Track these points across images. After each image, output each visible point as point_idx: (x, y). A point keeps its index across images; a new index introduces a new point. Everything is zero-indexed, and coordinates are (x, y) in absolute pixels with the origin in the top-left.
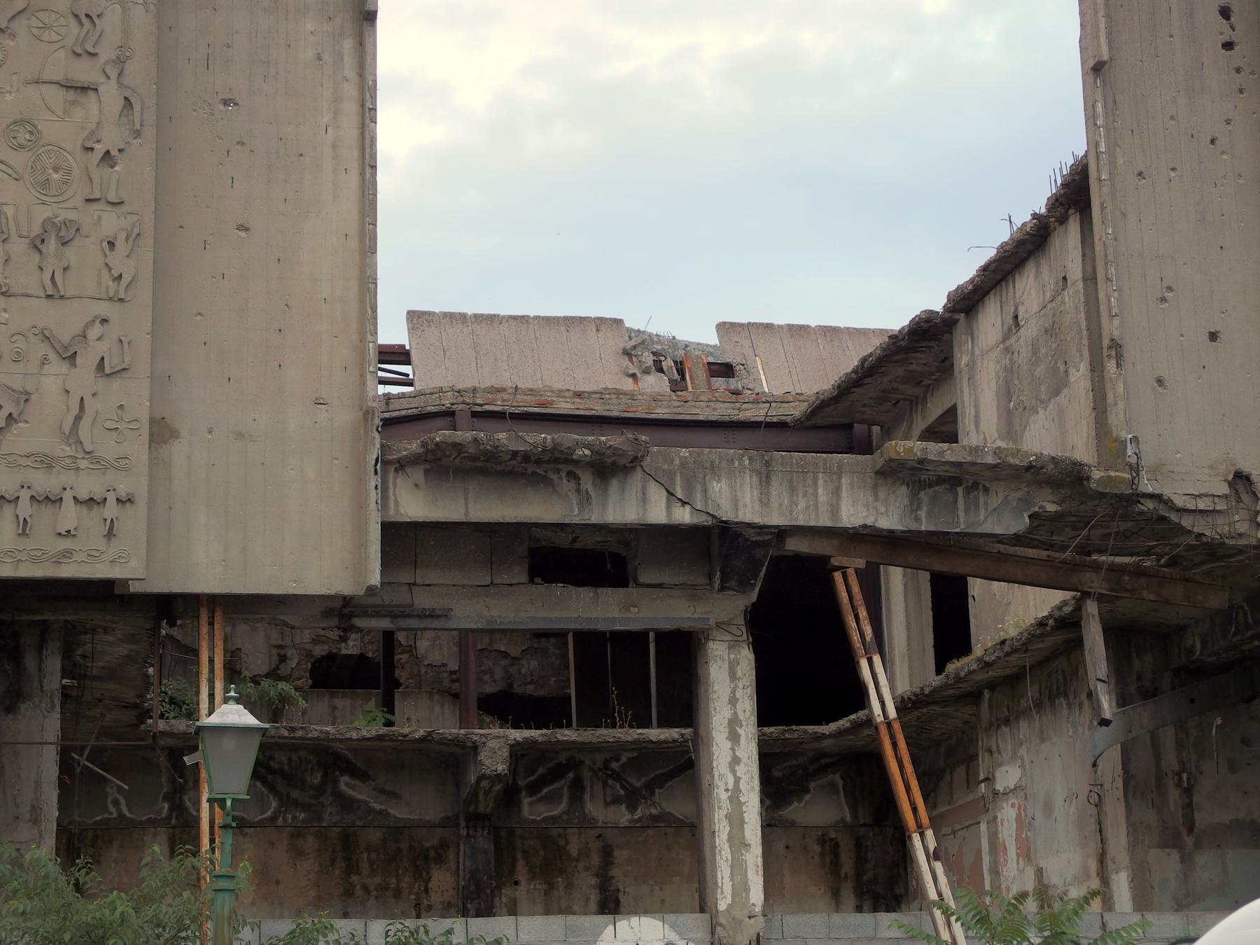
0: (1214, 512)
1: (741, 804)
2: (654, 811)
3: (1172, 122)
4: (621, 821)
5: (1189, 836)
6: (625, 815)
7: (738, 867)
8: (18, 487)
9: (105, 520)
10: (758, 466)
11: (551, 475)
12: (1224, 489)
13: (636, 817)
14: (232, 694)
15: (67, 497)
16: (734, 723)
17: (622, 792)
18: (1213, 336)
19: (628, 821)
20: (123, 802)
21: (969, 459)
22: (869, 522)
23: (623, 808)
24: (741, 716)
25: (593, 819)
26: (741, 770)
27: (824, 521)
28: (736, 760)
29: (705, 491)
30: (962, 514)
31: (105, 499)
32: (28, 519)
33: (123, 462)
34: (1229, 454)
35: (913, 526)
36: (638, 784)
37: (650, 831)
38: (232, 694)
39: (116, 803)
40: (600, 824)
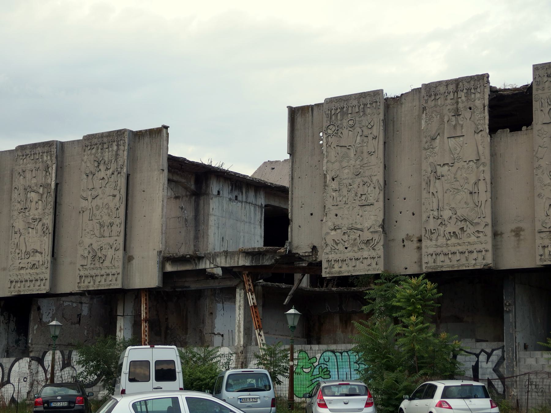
1: (240, 323)
7: (239, 337)
10: (225, 254)
11: (191, 260)
16: (240, 306)
18: (312, 214)
20: (329, 308)
21: (253, 251)
22: (244, 264)
24: (241, 305)
26: (240, 316)
27: (236, 265)
28: (240, 314)
29: (216, 261)
30: (261, 261)
35: (252, 264)
39: (328, 308)
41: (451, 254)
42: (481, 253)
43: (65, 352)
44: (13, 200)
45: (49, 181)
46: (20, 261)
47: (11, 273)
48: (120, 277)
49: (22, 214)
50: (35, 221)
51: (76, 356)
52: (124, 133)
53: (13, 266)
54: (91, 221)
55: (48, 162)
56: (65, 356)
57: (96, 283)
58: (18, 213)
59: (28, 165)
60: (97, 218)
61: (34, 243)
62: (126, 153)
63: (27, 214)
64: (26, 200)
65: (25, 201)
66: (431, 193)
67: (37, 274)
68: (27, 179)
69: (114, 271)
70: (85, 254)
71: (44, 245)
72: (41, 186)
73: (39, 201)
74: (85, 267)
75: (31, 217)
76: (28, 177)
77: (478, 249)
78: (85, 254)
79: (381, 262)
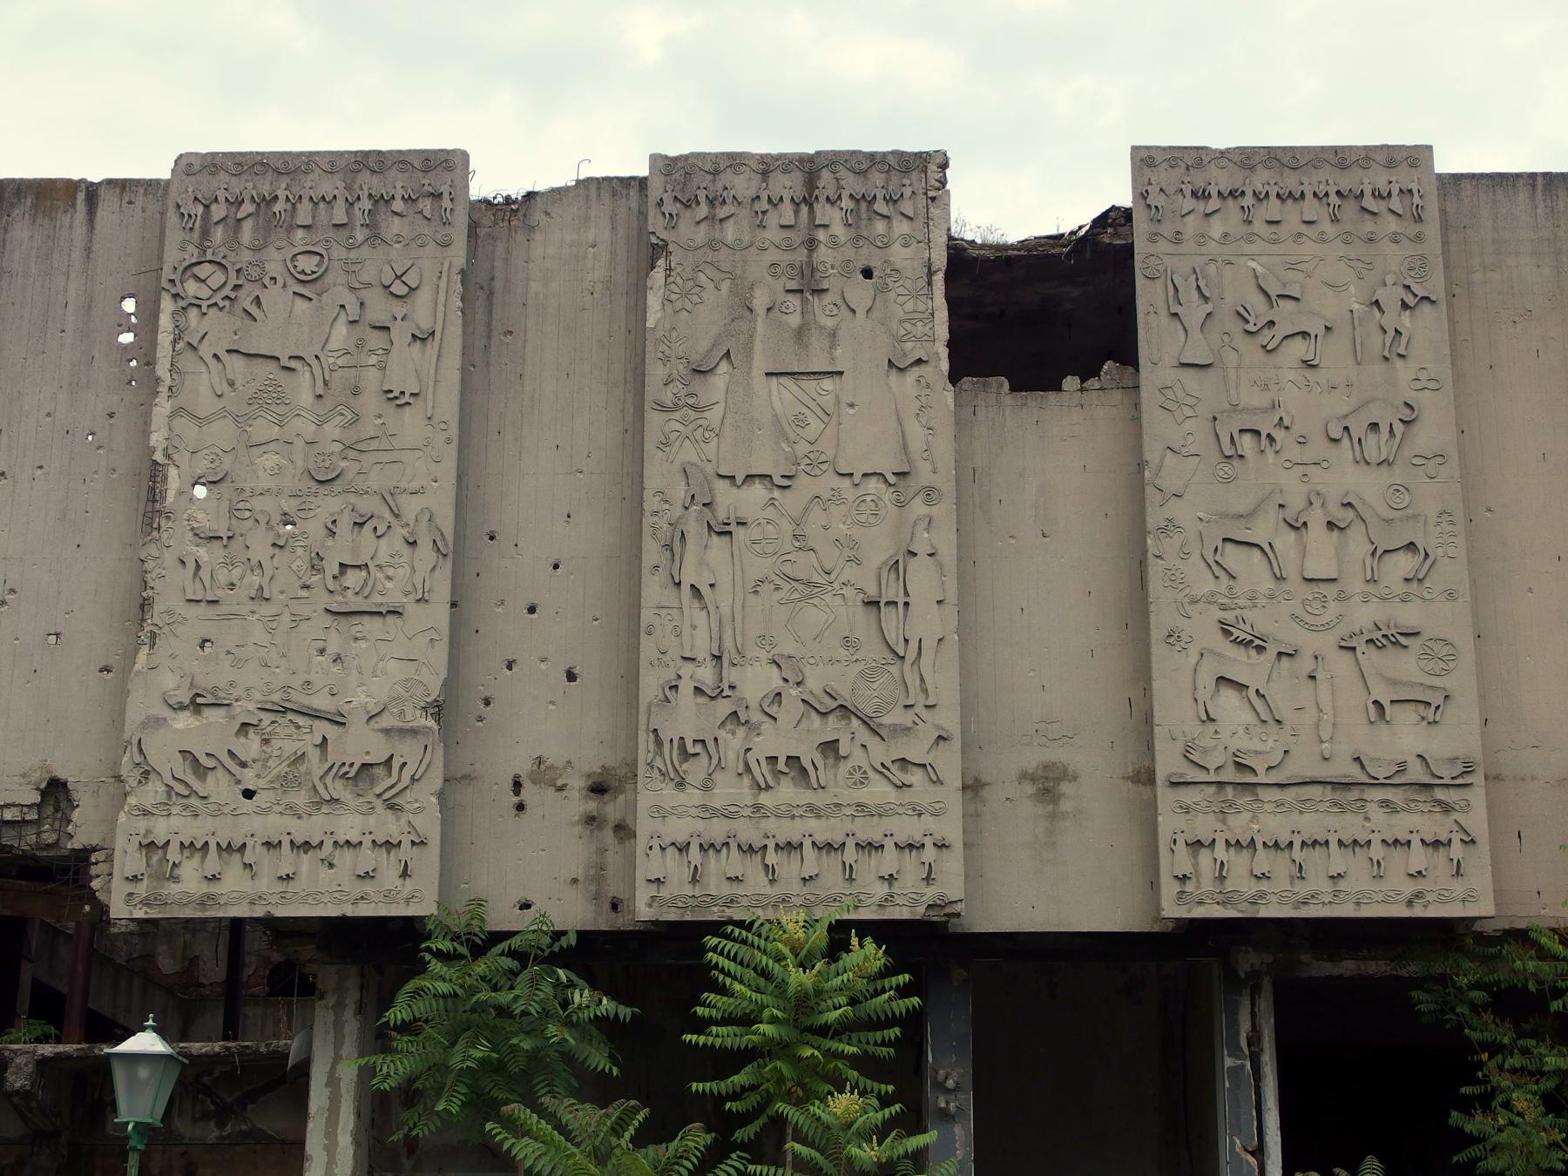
0: (24, 822)
2: (244, 1127)
3: (48, 419)
4: (209, 1137)
5: (408, 1159)
6: (213, 1131)
8: (801, 836)
9: (1452, 860)
12: (36, 798)
13: (224, 1134)
14: (150, 1022)
15: (889, 844)
17: (212, 1107)
19: (216, 1137)
23: (212, 1124)
25: (179, 1135)
31: (1450, 840)
32: (853, 865)
33: (937, 806)
34: (46, 761)
36: (229, 1100)
37: (238, 1148)
38: (150, 1022)
40: (187, 1141)
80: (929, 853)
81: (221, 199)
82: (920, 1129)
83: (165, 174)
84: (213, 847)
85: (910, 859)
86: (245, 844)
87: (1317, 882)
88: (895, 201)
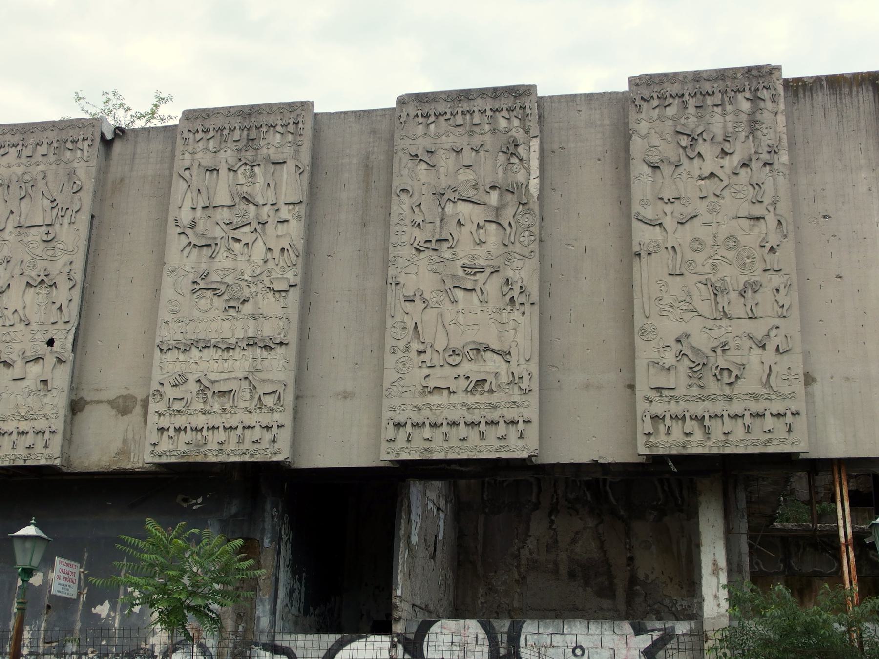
9: (786, 424)
15: (767, 413)
32: (484, 432)
41: (207, 431)
42: (515, 425)
43: (496, 624)
44: (394, 219)
45: (521, 177)
46: (426, 371)
47: (395, 402)
48: (58, 440)
49: (427, 253)
50: (475, 273)
51: (536, 637)
52: (771, 73)
53: (402, 383)
54: (678, 278)
55: (513, 133)
56: (499, 636)
57: (713, 437)
58: (414, 250)
59: (444, 137)
60: (700, 269)
61: (475, 328)
62: (781, 119)
63: (447, 255)
64: (442, 220)
65: (438, 223)
66: (669, 249)
67: (493, 407)
68: (442, 170)
69: (41, 424)
70: (664, 360)
71: (513, 332)
72: (493, 188)
73: (487, 224)
74: (666, 393)
75: (459, 263)
76: (443, 164)
77: (38, 428)
78: (664, 360)
79: (57, 442)
80: (789, 419)
81: (655, 97)
82: (259, 568)
83: (394, 105)
84: (189, 429)
85: (512, 428)
86: (704, 416)
87: (454, 442)
88: (286, 126)
